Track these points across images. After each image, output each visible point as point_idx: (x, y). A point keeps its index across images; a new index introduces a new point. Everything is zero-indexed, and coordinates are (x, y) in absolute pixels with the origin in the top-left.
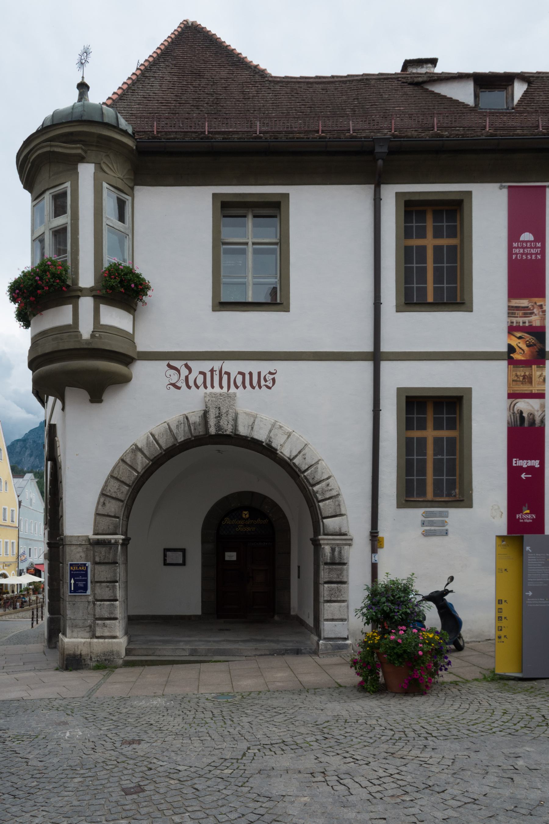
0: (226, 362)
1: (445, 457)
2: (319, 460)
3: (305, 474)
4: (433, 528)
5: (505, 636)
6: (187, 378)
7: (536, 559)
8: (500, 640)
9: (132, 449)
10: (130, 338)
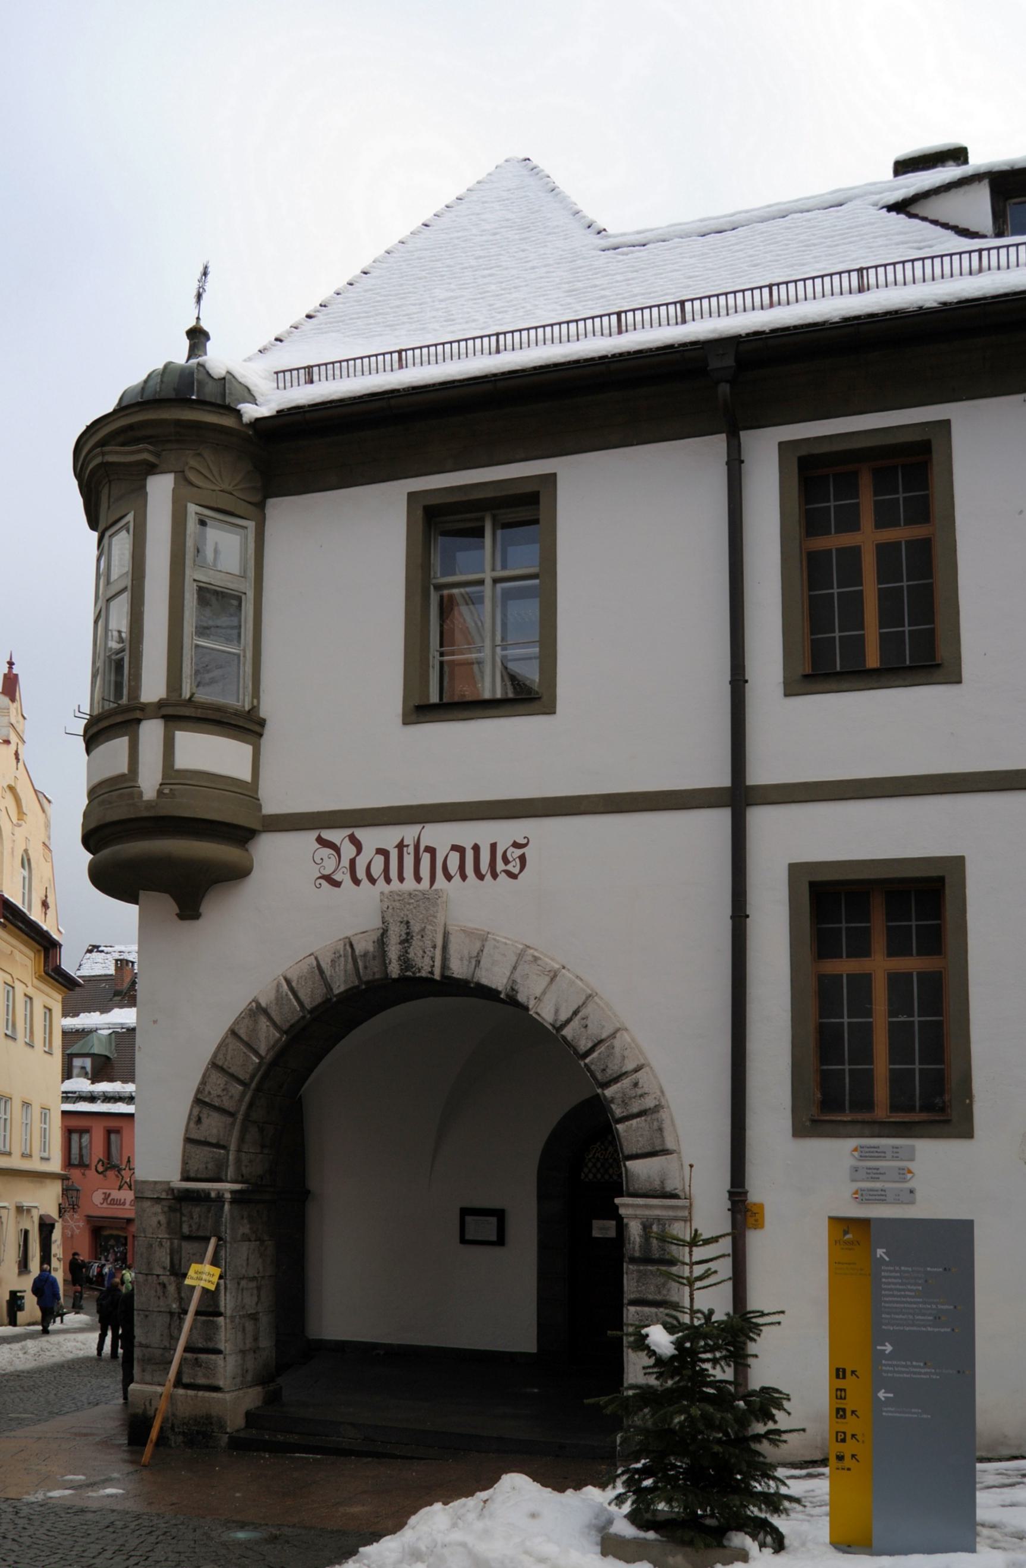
0: (429, 827)
1: (916, 1019)
2: (617, 1030)
3: (587, 1061)
4: (878, 1185)
5: (853, 1456)
6: (353, 862)
7: (900, 1277)
8: (840, 1465)
9: (250, 1010)
10: (247, 792)
